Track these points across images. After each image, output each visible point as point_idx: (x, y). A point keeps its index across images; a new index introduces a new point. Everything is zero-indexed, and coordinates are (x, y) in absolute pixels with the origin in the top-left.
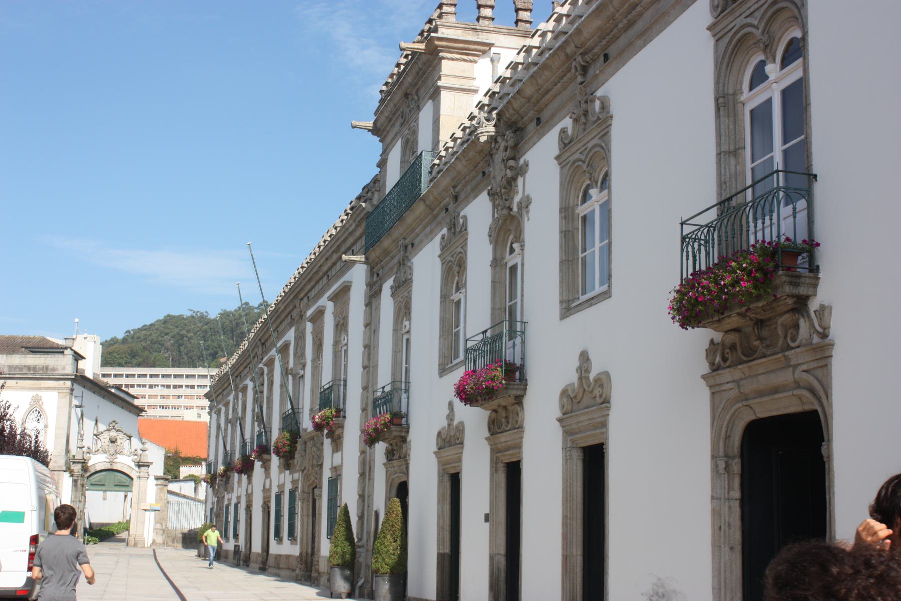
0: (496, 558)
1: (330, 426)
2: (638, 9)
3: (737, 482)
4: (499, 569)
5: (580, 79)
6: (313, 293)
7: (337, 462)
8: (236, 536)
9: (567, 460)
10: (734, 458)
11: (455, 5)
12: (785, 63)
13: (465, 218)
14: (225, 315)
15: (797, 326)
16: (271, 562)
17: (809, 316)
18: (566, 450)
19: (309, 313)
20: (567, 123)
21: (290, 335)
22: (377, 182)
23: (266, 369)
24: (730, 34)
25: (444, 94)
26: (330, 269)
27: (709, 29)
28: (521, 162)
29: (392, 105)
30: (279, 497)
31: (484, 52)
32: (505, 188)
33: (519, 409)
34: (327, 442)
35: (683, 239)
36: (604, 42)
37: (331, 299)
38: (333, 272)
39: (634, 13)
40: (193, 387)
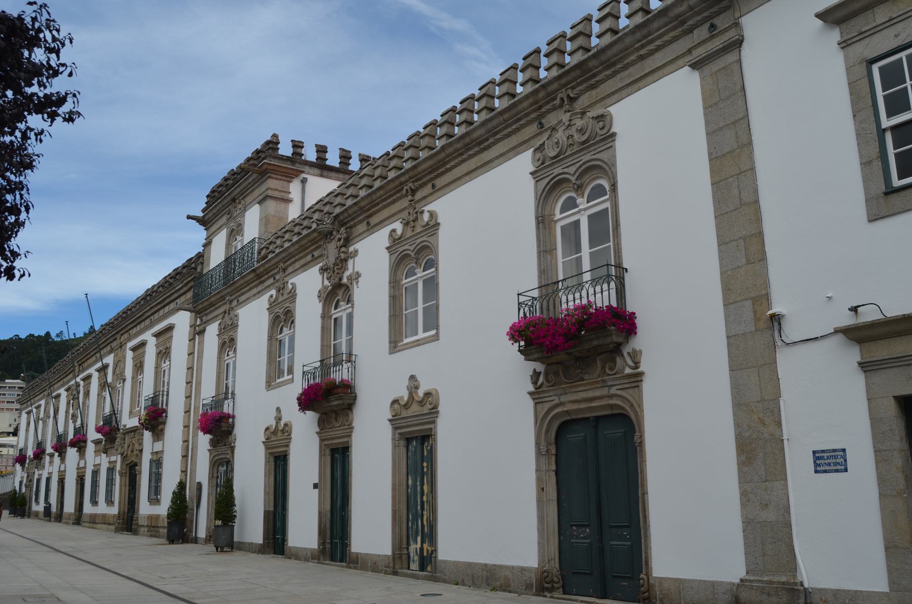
1: (155, 419)
6: (134, 331)
7: (158, 446)
13: (294, 285)
16: (84, 519)
17: (623, 355)
20: (398, 226)
21: (109, 360)
22: (200, 258)
23: (82, 383)
24: (578, 165)
27: (532, 174)
28: (351, 249)
30: (95, 473)
31: (297, 176)
35: (519, 304)
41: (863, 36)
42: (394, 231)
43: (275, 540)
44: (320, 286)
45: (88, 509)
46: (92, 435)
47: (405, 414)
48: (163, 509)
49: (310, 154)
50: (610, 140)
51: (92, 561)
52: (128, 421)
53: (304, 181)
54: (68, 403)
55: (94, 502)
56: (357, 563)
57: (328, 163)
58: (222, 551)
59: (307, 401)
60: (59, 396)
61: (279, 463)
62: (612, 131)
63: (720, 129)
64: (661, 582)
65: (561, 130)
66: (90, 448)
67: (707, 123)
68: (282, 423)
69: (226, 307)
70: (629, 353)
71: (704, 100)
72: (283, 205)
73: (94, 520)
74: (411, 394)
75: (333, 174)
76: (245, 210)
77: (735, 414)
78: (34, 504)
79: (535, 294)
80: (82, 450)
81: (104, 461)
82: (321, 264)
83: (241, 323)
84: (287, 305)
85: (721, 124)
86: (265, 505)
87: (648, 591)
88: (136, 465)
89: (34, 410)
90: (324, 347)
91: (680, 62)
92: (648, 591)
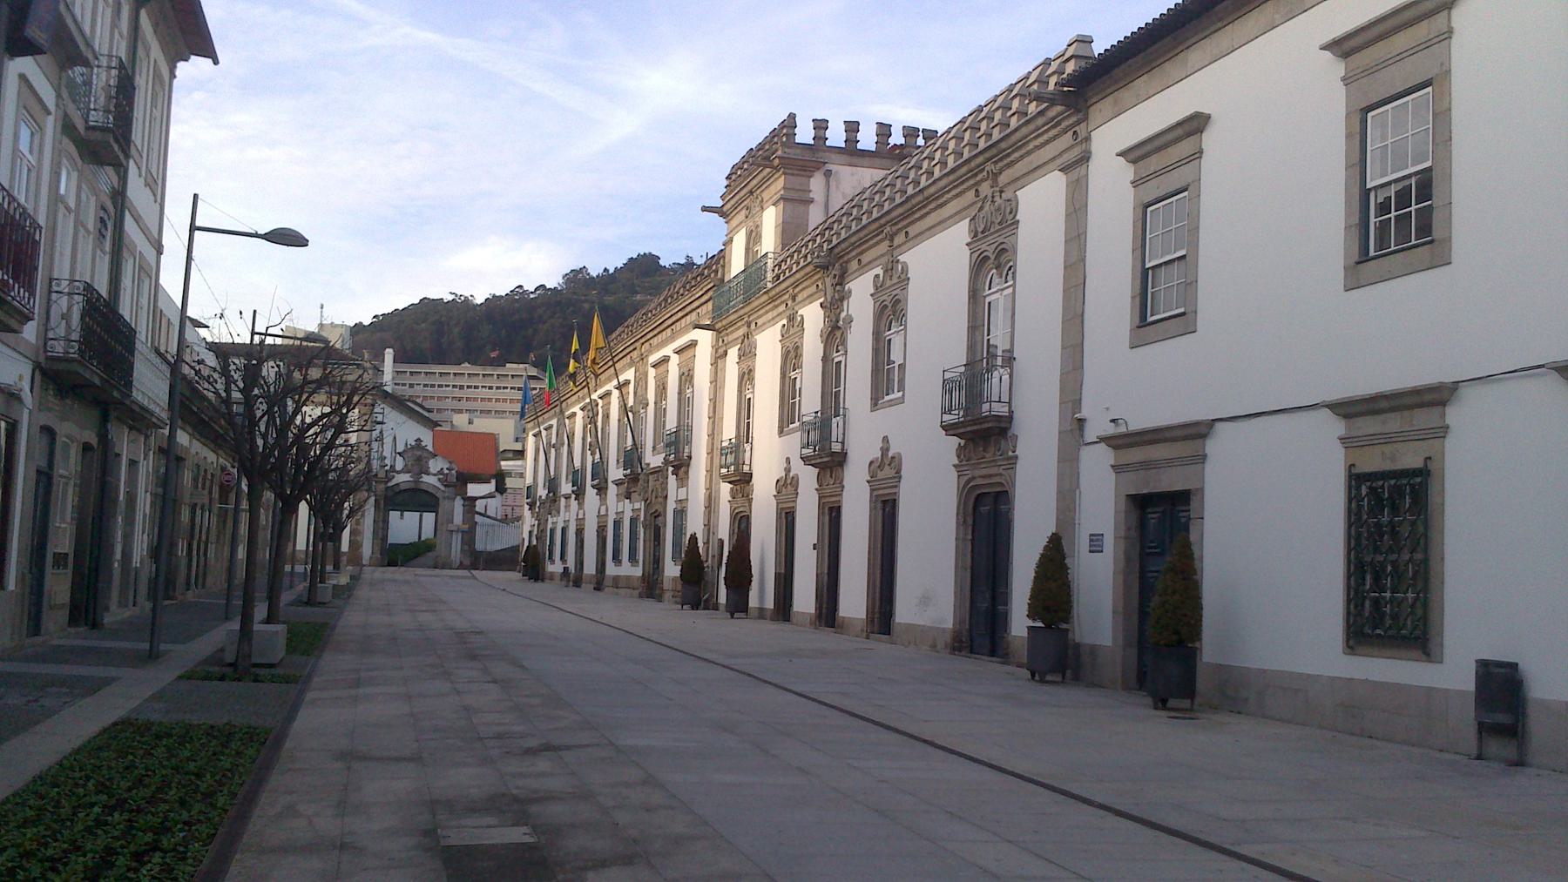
7: (682, 494)
8: (563, 557)
14: (493, 301)
16: (607, 582)
19: (653, 358)
21: (629, 375)
30: (618, 524)
34: (672, 479)
40: (461, 387)
41: (1369, 71)
42: (877, 276)
43: (828, 611)
45: (611, 569)
46: (615, 472)
47: (880, 475)
49: (836, 137)
51: (1165, 838)
52: (654, 460)
53: (828, 174)
54: (585, 427)
55: (617, 558)
57: (859, 146)
58: (1043, 681)
60: (574, 414)
61: (787, 520)
66: (612, 490)
69: (741, 332)
72: (801, 208)
73: (617, 582)
75: (866, 161)
78: (548, 563)
80: (601, 489)
81: (628, 508)
84: (1001, 240)
89: (544, 433)
90: (972, 347)
91: (1051, 166)
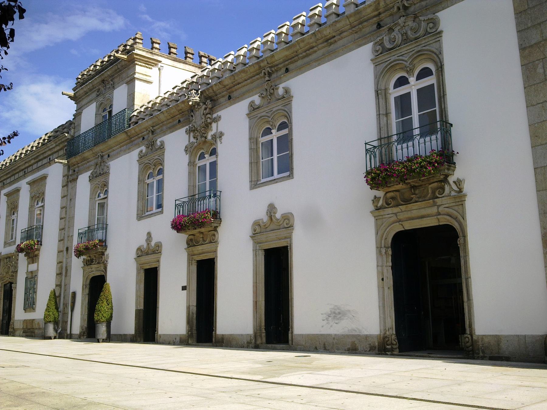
0: (191, 308)
2: (315, 49)
3: (390, 258)
4: (193, 313)
5: (267, 78)
9: (255, 255)
10: (388, 248)
11: (142, 40)
12: (418, 78)
15: (443, 189)
17: (449, 184)
18: (255, 251)
22: (70, 125)
24: (387, 63)
25: (137, 82)
26: (27, 167)
28: (215, 115)
29: (91, 85)
31: (156, 65)
32: (204, 127)
33: (215, 233)
36: (287, 63)
37: (28, 183)
38: (30, 169)
39: (311, 50)
44: (187, 143)
48: (39, 313)
50: (438, 36)
56: (223, 342)
59: (178, 226)
62: (439, 30)
63: (528, 28)
64: (482, 338)
65: (396, 30)
67: (518, 24)
68: (153, 244)
70: (454, 182)
71: (515, 9)
74: (271, 218)
76: (114, 88)
77: (541, 221)
79: (375, 144)
82: (187, 127)
83: (112, 171)
85: (529, 25)
86: (136, 305)
87: (472, 345)
88: (11, 283)
90: (191, 186)
92: (472, 345)
